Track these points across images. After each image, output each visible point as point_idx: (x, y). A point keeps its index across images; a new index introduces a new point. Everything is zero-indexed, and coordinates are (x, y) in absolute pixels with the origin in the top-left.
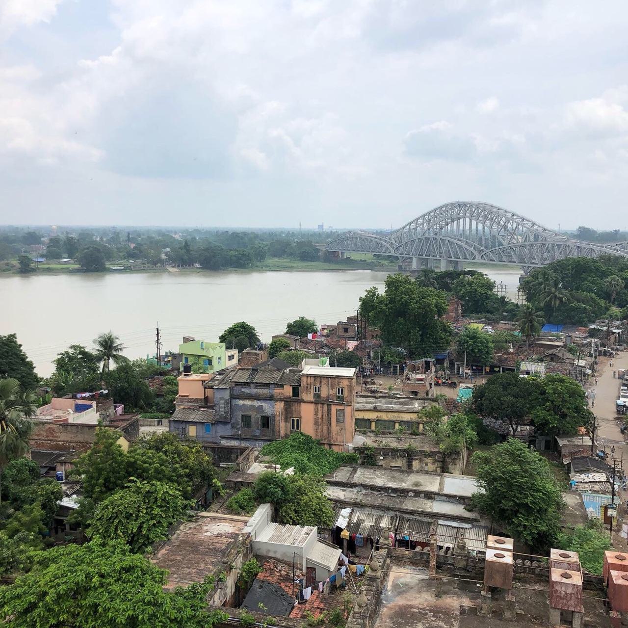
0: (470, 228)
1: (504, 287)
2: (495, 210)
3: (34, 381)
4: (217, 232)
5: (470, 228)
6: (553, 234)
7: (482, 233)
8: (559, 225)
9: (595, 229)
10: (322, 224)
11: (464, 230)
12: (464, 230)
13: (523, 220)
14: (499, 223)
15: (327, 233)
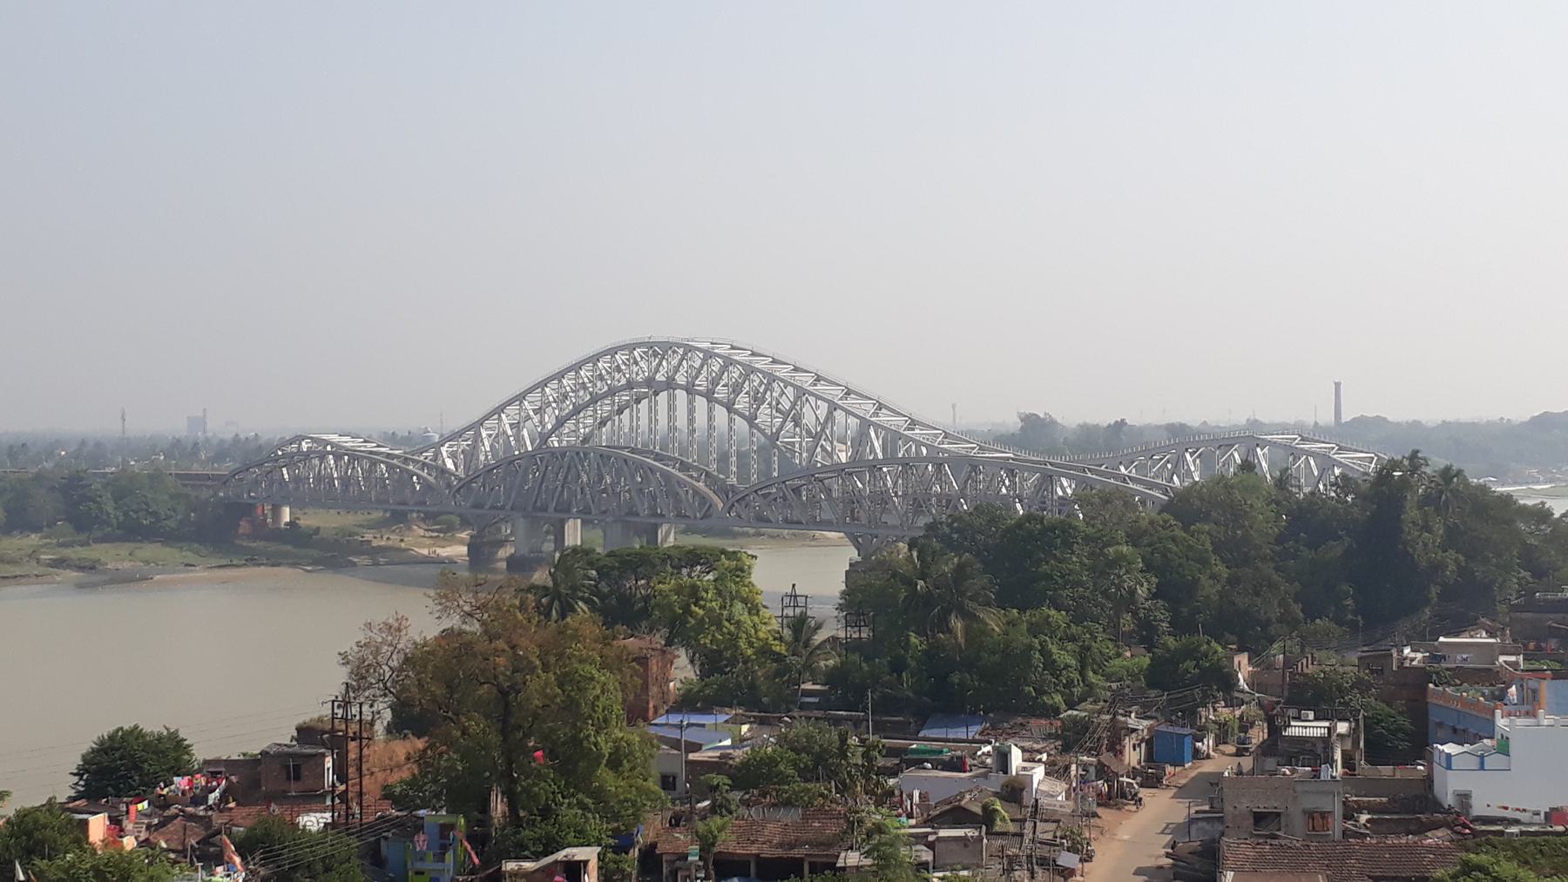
0: (691, 420)
1: (801, 601)
2: (761, 364)
3: (775, 639)
4: (393, 433)
5: (691, 420)
6: (936, 436)
7: (685, 435)
8: (954, 407)
9: (1400, 420)
10: (200, 414)
11: (672, 428)
12: (672, 428)
13: (848, 393)
14: (778, 403)
15: (222, 441)
